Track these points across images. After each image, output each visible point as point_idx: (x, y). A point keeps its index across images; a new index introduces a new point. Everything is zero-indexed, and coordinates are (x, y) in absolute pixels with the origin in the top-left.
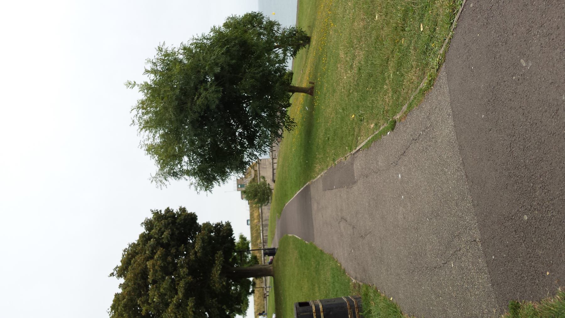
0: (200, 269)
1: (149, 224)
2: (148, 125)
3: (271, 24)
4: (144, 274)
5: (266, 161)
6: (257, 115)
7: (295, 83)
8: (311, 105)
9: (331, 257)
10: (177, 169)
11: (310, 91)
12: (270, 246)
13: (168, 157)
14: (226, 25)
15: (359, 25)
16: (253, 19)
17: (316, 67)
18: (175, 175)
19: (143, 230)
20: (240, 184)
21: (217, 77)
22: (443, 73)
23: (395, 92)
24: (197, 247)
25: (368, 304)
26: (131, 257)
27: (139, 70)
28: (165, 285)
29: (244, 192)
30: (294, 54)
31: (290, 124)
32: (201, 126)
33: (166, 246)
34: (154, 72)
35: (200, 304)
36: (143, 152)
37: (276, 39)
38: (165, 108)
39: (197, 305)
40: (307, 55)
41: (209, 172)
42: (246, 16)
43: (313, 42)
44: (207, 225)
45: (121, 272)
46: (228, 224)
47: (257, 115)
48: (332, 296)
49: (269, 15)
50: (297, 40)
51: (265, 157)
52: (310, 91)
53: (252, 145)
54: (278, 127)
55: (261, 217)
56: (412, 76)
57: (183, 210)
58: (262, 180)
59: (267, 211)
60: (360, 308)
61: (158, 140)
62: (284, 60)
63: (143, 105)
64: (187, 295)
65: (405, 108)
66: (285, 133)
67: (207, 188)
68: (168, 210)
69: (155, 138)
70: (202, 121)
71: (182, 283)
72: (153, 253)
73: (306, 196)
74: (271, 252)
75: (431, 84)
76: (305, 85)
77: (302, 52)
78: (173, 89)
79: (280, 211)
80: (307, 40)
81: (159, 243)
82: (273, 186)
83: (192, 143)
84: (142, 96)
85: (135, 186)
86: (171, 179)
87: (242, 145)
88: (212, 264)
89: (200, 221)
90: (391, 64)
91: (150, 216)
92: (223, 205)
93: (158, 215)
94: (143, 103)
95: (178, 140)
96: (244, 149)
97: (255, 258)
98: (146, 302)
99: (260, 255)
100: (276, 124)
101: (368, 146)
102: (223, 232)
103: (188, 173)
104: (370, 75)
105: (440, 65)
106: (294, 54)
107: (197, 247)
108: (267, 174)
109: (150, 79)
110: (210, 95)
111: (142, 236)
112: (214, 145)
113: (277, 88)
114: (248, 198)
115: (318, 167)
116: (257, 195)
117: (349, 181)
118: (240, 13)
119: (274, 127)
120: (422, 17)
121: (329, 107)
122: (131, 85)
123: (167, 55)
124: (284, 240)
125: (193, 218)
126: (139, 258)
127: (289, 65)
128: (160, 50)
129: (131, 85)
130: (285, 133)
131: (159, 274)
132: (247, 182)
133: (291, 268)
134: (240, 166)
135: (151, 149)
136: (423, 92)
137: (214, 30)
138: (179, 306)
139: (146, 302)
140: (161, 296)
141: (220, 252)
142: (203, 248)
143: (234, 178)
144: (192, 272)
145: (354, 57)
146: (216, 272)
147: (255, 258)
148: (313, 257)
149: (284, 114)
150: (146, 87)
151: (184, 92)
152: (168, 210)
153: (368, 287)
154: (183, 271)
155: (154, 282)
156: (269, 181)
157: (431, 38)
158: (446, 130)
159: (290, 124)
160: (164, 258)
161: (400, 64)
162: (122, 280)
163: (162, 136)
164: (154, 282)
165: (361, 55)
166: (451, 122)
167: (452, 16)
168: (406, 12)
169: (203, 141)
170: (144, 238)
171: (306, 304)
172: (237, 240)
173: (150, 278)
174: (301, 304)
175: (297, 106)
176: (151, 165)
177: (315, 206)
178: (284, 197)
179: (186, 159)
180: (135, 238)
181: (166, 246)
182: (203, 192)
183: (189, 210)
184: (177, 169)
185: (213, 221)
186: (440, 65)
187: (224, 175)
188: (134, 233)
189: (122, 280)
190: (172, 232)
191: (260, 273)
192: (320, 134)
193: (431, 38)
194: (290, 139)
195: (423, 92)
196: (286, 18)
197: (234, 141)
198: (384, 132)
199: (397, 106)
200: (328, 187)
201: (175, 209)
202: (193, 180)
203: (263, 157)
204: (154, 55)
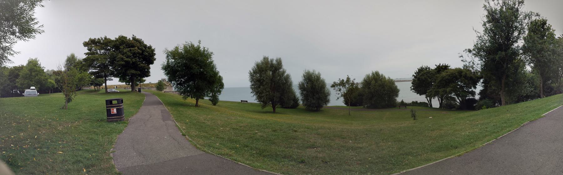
0: (134, 66)
1: (150, 47)
2: (185, 47)
3: (220, 92)
4: (133, 46)
5: (172, 89)
6: (188, 86)
7: (200, 100)
8: (192, 106)
9: (137, 112)
10: (170, 57)
11: (197, 105)
12: (142, 90)
13: (174, 54)
14: (220, 76)
15: (219, 122)
16: (222, 86)
17: (205, 108)
18: (168, 57)
19: (148, 45)
20: (164, 80)
21: (202, 72)
22: (202, 152)
23: (196, 136)
24: (142, 65)
25: (122, 123)
26: (139, 42)
27: (205, 45)
28: (129, 54)
29: (161, 81)
30: (210, 100)
31: (185, 98)
32: (185, 66)
33: (142, 54)
34: (204, 51)
35: (123, 66)
36: (176, 45)
37: (215, 94)
38: (191, 54)
39: (122, 65)
40: (210, 105)
41: (168, 69)
42: (456, 69)
43: (214, 106)
44: (149, 68)
45: (134, 39)
46: (150, 76)
47: (188, 86)
48: (125, 111)
49: (223, 91)
50: (214, 101)
51: (173, 89)
52: (197, 105)
53: (178, 84)
54: (184, 94)
55: (152, 87)
56: (201, 141)
57: (155, 59)
58: (487, 25)
59: (154, 89)
60: (121, 120)
61: (180, 51)
62: (208, 96)
63: (192, 46)
64: (125, 61)
65: (190, 139)
66: (182, 96)
67: (163, 68)
68: (155, 54)
69: (181, 50)
70: (187, 67)
71: (130, 60)
72: (140, 49)
73: (160, 103)
74: (140, 91)
75: (197, 148)
76: (199, 103)
77: (211, 102)
78: (198, 57)
79: (154, 94)
80: (215, 104)
81: (143, 51)
82: (163, 92)
83: (179, 63)
84: (196, 46)
85: (163, 41)
86: (166, 55)
87: (178, 81)
88: (136, 70)
89: (151, 66)
90: (205, 134)
91: (153, 48)
92: (157, 73)
93: (153, 50)
94: (193, 46)
95: (180, 58)
96: (176, 81)
97: (138, 85)
98: (124, 48)
99: (139, 87)
100: (185, 93)
101: (177, 126)
102: (147, 74)
103: (168, 61)
104: (202, 127)
105: (205, 151)
106: (210, 100)
107: (142, 65)
108: (167, 90)
109: (202, 49)
110: (196, 69)
111: (146, 45)
112: (178, 71)
113: (198, 93)
114: (159, 83)
115: (169, 108)
116: (160, 86)
117: (164, 119)
118: (224, 81)
119: (184, 93)
120: (221, 144)
121: (191, 112)
122: (200, 42)
123: (210, 55)
124: (144, 95)
125: (152, 63)
126: (138, 44)
127: (206, 98)
128: (212, 53)
129: (200, 42)
130: (182, 96)
131: (133, 52)
132: (165, 82)
133: (134, 97)
134: (170, 80)
135: (177, 48)
136: (195, 146)
137: (218, 72)
138: (122, 59)
139: (124, 48)
140: (126, 53)
141: (139, 73)
142: (142, 67)
143: (166, 78)
144: (133, 63)
145: (208, 121)
146: (133, 71)
147: (138, 85)
148: (138, 105)
149: (189, 96)
150: (199, 47)
151: (197, 61)
152: (155, 54)
153: (127, 124)
154: (134, 60)
155: (130, 50)
156: (165, 90)
157: (214, 148)
158: (182, 154)
159: (185, 98)
160: (139, 53)
161: (205, 137)
162: (131, 39)
163: (181, 52)
164: (130, 50)
165: (209, 123)
166: (185, 156)
167: (221, 154)
168: (223, 138)
169: (180, 67)
170: (145, 46)
171: (122, 102)
172: (144, 79)
173: (132, 49)
174: (122, 100)
175: (191, 101)
176: (171, 48)
177: (155, 106)
178: (159, 95)
179: (173, 61)
180: (145, 43)
181: (142, 54)
182: (161, 67)
183: (155, 62)
184: (170, 57)
185: (151, 70)
186: (205, 151)
187: (167, 74)
188: (147, 43)
189: (131, 39)
190: (147, 56)
191: (132, 87)
192: (181, 109)
193: (214, 148)
194: (180, 98)
195: (195, 146)
196: (222, 97)
197: (179, 78)
198: (181, 132)
199: (191, 137)
200: (162, 112)
201: (155, 57)
202: (166, 63)
203: (173, 88)
204: (210, 51)
